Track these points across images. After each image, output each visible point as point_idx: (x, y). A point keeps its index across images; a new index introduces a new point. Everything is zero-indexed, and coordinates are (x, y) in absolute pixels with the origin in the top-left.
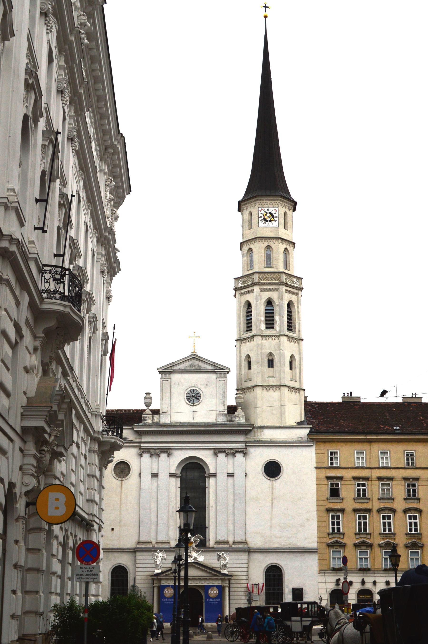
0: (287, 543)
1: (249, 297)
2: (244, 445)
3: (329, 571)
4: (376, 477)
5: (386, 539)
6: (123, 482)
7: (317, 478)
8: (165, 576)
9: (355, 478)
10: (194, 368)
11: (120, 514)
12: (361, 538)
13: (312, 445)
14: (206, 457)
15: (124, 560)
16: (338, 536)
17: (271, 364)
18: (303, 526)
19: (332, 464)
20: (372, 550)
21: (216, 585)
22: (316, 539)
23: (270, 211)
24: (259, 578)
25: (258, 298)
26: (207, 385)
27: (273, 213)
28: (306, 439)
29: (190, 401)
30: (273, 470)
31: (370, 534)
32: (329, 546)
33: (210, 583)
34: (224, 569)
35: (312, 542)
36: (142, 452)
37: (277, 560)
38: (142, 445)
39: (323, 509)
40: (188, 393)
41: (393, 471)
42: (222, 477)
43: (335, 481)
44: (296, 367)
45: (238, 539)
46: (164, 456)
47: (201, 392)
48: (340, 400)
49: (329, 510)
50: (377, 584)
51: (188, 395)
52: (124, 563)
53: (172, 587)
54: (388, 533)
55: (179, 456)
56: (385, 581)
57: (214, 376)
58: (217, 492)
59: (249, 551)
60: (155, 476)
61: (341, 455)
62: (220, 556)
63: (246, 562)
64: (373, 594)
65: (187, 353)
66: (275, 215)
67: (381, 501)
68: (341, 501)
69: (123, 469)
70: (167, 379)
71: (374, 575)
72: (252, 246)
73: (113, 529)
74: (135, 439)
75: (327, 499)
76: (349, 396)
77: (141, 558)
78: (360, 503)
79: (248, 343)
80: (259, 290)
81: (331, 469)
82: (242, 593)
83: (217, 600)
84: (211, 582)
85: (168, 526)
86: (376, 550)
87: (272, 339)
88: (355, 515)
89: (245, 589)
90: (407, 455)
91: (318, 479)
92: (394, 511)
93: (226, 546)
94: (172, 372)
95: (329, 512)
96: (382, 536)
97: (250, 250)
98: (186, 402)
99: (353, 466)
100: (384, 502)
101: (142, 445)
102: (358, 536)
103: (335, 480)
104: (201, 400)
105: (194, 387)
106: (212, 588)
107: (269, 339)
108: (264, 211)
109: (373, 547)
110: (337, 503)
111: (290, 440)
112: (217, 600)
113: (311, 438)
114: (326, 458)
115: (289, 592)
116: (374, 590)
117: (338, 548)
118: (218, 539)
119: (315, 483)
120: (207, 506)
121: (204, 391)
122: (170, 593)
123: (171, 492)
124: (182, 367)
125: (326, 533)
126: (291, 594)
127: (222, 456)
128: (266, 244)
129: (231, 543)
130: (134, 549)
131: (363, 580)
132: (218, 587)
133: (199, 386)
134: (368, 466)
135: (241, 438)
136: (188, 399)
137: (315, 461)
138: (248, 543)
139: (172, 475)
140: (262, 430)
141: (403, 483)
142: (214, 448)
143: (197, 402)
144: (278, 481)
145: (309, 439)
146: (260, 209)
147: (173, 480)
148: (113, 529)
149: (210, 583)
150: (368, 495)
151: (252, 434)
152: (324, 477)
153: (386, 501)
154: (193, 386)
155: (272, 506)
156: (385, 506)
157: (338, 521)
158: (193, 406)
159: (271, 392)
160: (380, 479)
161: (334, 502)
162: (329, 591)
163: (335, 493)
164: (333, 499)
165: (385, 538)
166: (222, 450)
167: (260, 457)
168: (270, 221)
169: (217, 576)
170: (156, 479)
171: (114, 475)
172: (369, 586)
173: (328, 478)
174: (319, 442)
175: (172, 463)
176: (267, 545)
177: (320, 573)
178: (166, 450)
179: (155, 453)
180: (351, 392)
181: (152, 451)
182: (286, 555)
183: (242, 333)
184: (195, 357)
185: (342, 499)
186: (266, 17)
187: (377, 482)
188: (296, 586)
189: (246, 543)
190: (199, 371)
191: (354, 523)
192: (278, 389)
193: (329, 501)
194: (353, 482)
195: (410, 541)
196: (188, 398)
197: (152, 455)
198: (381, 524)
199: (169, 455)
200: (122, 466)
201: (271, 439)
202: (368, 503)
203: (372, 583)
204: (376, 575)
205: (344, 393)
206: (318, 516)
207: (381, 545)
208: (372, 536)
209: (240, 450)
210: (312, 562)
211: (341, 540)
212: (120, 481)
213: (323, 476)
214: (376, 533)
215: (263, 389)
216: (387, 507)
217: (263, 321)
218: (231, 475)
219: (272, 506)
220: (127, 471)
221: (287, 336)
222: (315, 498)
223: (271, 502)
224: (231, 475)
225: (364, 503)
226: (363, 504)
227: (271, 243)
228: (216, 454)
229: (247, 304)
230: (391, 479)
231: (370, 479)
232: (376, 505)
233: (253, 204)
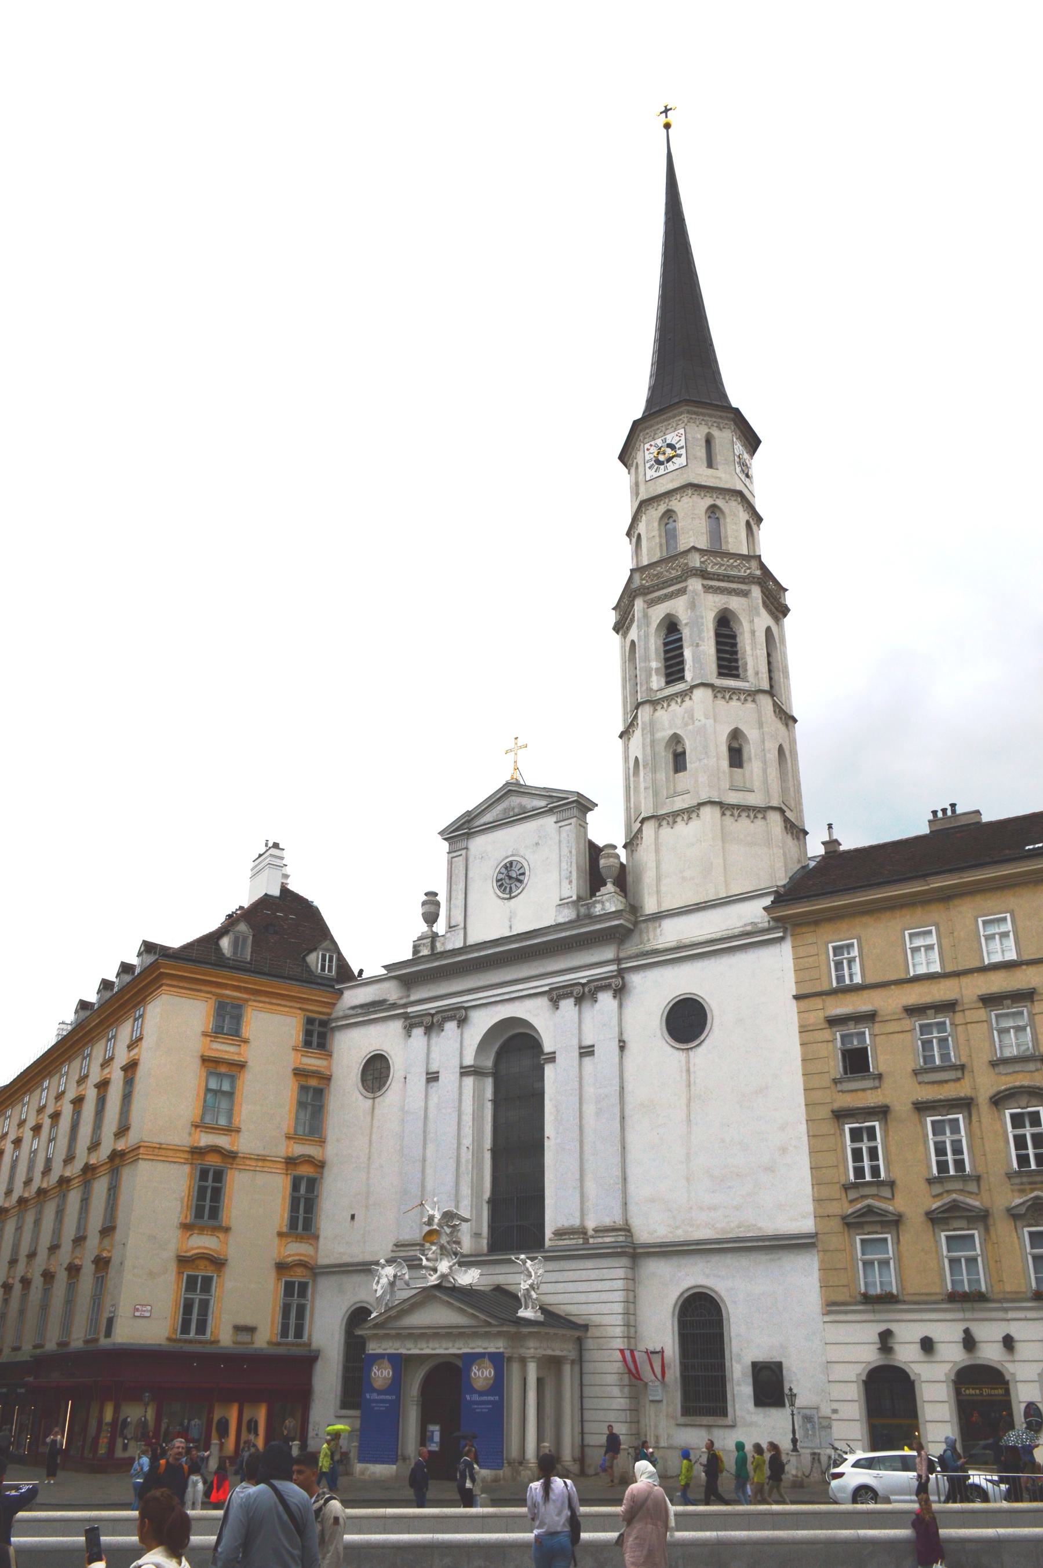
0: (732, 1225)
2: (614, 967)
3: (855, 1304)
4: (975, 998)
5: (1033, 1190)
6: (377, 1100)
7: (801, 1026)
9: (912, 1011)
10: (511, 814)
11: (368, 1179)
12: (947, 1191)
13: (781, 939)
14: (535, 1012)
16: (873, 1190)
18: (770, 1169)
19: (840, 978)
20: (987, 1230)
21: (389, 1355)
22: (809, 1207)
23: (668, 442)
24: (661, 1333)
26: (537, 844)
28: (766, 925)
30: (687, 1021)
31: (978, 1179)
32: (852, 1223)
33: (479, 1347)
37: (708, 1276)
38: (409, 1010)
39: (825, 1112)
40: (499, 872)
43: (852, 1029)
44: (750, 759)
47: (525, 865)
48: (925, 830)
49: (840, 1115)
50: (1018, 1346)
53: (390, 1361)
55: (482, 1022)
56: (1000, 1337)
57: (549, 821)
61: (865, 951)
63: (620, 1284)
64: (1007, 1383)
66: (678, 446)
67: (1002, 1069)
68: (877, 1083)
69: (376, 1071)
70: (459, 853)
71: (1001, 1315)
73: (353, 1217)
74: (401, 998)
75: (835, 1081)
76: (949, 813)
78: (929, 1083)
81: (840, 996)
82: (612, 1379)
83: (388, 1397)
84: (479, 1343)
86: (1002, 1227)
87: (677, 702)
88: (921, 1122)
89: (618, 1366)
91: (803, 1030)
93: (574, 1242)
94: (469, 835)
95: (841, 1120)
96: (1017, 1181)
98: (499, 896)
99: (903, 976)
100: (1011, 1070)
101: (409, 1010)
102: (937, 1189)
103: (851, 1024)
104: (525, 882)
105: (512, 855)
106: (478, 1361)
107: (669, 705)
108: (656, 446)
109: (991, 1221)
110: (864, 1090)
111: (725, 934)
112: (388, 1397)
114: (824, 967)
115: (743, 1374)
116: (1012, 1370)
117: (878, 1228)
119: (796, 1039)
122: (385, 1378)
124: (488, 817)
125: (838, 1186)
126: (750, 1380)
128: (708, 501)
132: (498, 1360)
133: (522, 852)
135: (608, 953)
137: (793, 980)
138: (633, 1231)
139: (465, 1071)
142: (546, 988)
143: (517, 888)
144: (700, 1050)
145: (772, 923)
148: (353, 1217)
149: (478, 1346)
150: (958, 1056)
151: (635, 938)
152: (822, 1020)
153: (1017, 1067)
154: (510, 853)
155: (689, 1120)
156: (1017, 1084)
157: (872, 1144)
158: (511, 898)
159: (680, 826)
161: (856, 1091)
163: (856, 1061)
164: (854, 1080)
165: (1028, 1187)
168: (669, 460)
169: (489, 1324)
171: (361, 1088)
172: (991, 1353)
173: (833, 1022)
174: (799, 925)
175: (461, 1045)
176: (679, 1232)
177: (829, 1313)
179: (432, 1024)
180: (953, 806)
182: (728, 1260)
185: (880, 1077)
186: (667, 126)
187: (982, 1014)
188: (761, 1357)
189: (629, 1231)
190: (524, 816)
191: (921, 1148)
193: (840, 1087)
194: (907, 1023)
196: (500, 884)
198: (1008, 1142)
201: (680, 941)
202: (958, 1080)
203: (918, 1346)
204: (1011, 1315)
205: (935, 813)
206: (812, 1136)
207: (1014, 1212)
209: (603, 983)
210: (802, 1280)
211: (883, 1205)
212: (371, 1101)
213: (817, 1017)
214: (995, 1175)
215: (660, 825)
216: (1021, 1087)
217: (657, 670)
219: (689, 1120)
221: (711, 686)
222: (797, 1082)
223: (684, 1107)
225: (946, 1081)
226: (947, 1086)
231: (958, 1008)
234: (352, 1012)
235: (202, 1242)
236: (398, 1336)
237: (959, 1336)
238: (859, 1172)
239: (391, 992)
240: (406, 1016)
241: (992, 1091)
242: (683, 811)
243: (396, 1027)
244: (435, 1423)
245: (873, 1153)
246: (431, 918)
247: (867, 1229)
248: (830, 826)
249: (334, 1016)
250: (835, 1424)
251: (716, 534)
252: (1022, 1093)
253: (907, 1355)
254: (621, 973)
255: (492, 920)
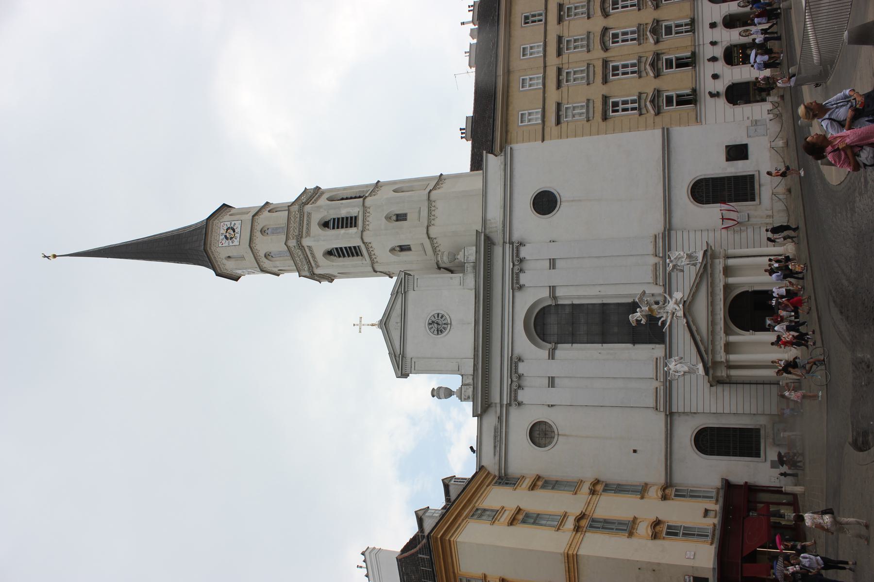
1: (319, 254)
2: (508, 245)
8: (707, 354)
9: (559, 86)
14: (525, 302)
15: (685, 432)
17: (401, 217)
22: (649, 132)
25: (321, 241)
27: (225, 228)
29: (445, 328)
34: (697, 259)
35: (657, 134)
36: (515, 401)
38: (505, 403)
39: (603, 125)
41: (549, 37)
42: (555, 278)
45: (650, 249)
46: (522, 368)
48: (470, 142)
49: (605, 118)
51: (436, 332)
52: (690, 433)
54: (639, 35)
55: (523, 345)
57: (411, 295)
58: (581, 287)
59: (668, 230)
60: (552, 382)
62: (674, 266)
65: (378, 333)
67: (591, 47)
71: (701, 47)
72: (262, 254)
73: (635, 451)
77: (681, 403)
79: (376, 252)
80: (308, 238)
82: (737, 236)
84: (717, 275)
85: (629, 364)
86: (661, 47)
90: (526, 23)
92: (605, 30)
97: (266, 256)
102: (644, 74)
103: (561, 113)
113: (501, 151)
118: (651, 280)
119: (564, 141)
120: (600, 302)
121: (430, 311)
123: (580, 359)
127: (524, 279)
128: (258, 234)
129: (656, 260)
130: (666, 415)
131: (709, 60)
134: (542, 71)
135: (498, 251)
136: (441, 331)
139: (552, 356)
140: (488, 222)
141: (566, 23)
146: (221, 248)
147: (558, 353)
148: (635, 451)
153: (591, 41)
159: (436, 213)
160: (559, 53)
162: (729, 106)
166: (515, 279)
167: (527, 223)
170: (557, 381)
172: (719, 52)
174: (506, 139)
175: (534, 357)
177: (701, 121)
178: (513, 365)
179: (517, 382)
180: (461, 129)
181: (514, 387)
182: (673, 175)
183: (364, 262)
184: (384, 324)
188: (723, 155)
192: (433, 204)
194: (564, 88)
195: (650, 3)
196: (439, 332)
197: (520, 387)
199: (520, 359)
200: (536, 434)
204: (701, 43)
206: (614, 131)
208: (643, 55)
209: (515, 252)
210: (686, 136)
218: (553, 264)
220: (543, 427)
224: (553, 264)
227: (258, 228)
228: (521, 287)
229: (328, 256)
230: (560, 39)
232: (598, 54)
233: (216, 254)
234: (497, 454)
235: (643, 529)
236: (713, 342)
237: (711, 63)
238: (633, 109)
239: (491, 420)
240: (509, 405)
241: (602, 52)
242: (429, 208)
243: (514, 412)
244: (765, 322)
245: (625, 66)
246: (448, 393)
247: (661, 104)
248: (463, 23)
249: (497, 474)
250: (755, 118)
251: (276, 231)
252: (604, 43)
253: (720, 86)
254: (511, 243)
255: (462, 339)
